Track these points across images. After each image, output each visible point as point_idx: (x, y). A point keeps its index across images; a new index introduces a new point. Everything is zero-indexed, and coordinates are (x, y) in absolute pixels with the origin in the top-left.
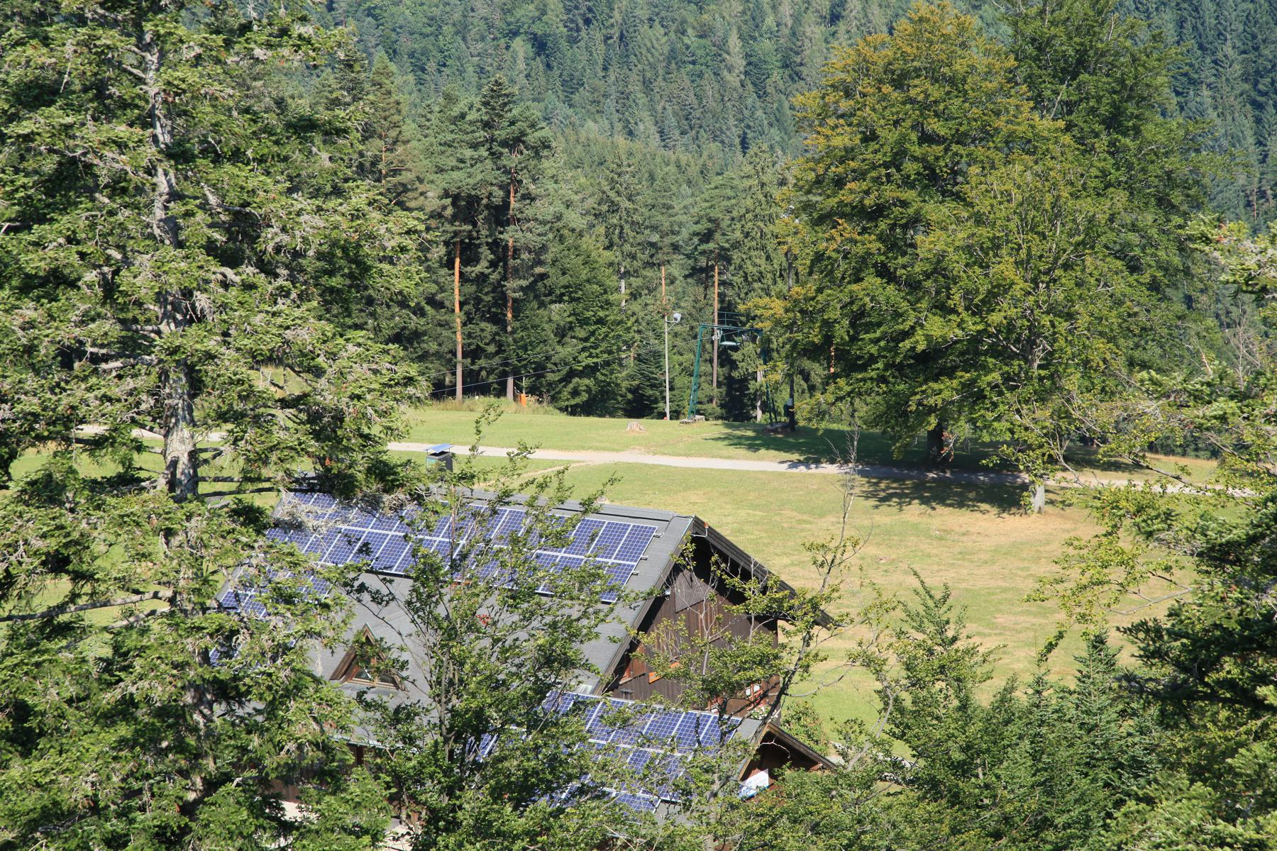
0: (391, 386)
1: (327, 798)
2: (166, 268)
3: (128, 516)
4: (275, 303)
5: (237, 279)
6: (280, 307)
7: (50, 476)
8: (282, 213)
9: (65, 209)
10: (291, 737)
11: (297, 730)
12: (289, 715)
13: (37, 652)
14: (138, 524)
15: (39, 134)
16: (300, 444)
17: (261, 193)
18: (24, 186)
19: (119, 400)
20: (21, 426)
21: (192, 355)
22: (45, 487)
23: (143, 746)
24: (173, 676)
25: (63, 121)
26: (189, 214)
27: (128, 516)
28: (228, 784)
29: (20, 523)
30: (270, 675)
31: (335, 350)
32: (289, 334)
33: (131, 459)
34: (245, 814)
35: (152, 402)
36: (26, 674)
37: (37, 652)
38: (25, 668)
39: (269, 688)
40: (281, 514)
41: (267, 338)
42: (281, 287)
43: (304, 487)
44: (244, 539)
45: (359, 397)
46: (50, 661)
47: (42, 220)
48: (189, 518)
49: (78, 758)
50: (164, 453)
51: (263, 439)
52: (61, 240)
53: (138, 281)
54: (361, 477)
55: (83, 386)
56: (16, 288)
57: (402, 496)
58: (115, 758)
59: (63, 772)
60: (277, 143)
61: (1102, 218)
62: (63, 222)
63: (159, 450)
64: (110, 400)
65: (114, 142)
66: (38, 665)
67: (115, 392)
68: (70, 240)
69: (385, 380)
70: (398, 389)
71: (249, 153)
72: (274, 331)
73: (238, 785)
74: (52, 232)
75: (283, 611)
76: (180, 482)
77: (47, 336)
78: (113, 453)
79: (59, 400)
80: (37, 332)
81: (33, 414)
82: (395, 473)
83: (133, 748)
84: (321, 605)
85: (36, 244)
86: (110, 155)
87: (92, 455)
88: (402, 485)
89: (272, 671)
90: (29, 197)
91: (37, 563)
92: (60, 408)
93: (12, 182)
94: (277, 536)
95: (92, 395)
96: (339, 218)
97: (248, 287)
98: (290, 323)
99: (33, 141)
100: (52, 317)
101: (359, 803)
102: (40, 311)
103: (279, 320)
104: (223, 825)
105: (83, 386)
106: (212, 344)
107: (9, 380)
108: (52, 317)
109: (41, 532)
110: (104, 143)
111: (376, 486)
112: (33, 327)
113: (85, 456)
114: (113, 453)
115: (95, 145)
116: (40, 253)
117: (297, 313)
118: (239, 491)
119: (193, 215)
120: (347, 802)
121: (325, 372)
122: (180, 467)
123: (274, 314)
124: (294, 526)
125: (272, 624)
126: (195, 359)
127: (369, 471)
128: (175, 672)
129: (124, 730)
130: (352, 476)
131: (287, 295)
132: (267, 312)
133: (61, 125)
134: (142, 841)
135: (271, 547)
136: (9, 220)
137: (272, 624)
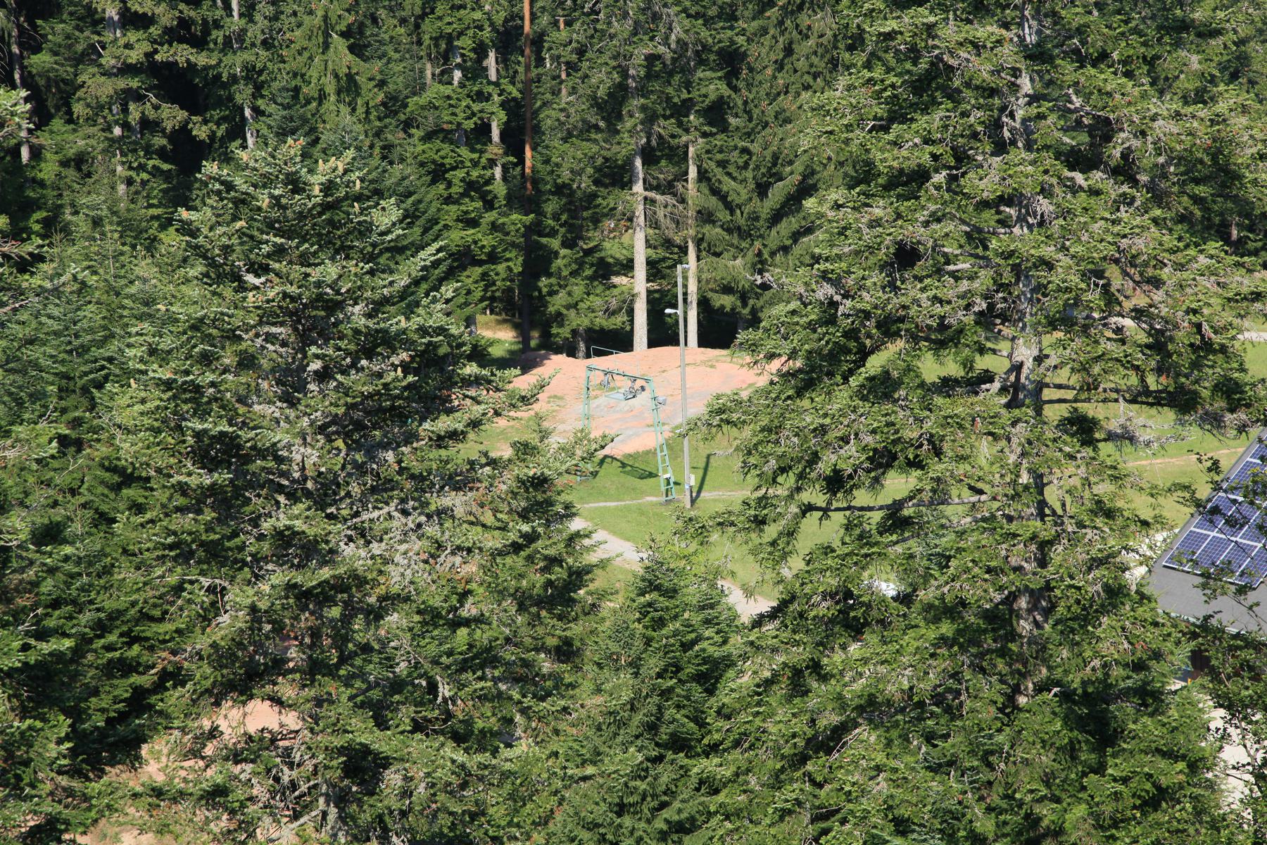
0: (1237, 301)
1: (1145, 719)
2: (1011, 172)
3: (951, 417)
4: (1118, 210)
5: (1084, 184)
6: (1123, 214)
7: (887, 372)
8: (1136, 118)
9: (927, 108)
10: (1097, 654)
11: (1104, 647)
12: (1099, 632)
13: (866, 544)
14: (961, 427)
15: (901, 33)
16: (1126, 356)
17: (1118, 96)
18: (893, 86)
19: (949, 302)
20: (853, 322)
21: (1028, 260)
22: (882, 383)
23: (961, 646)
24: (986, 580)
25: (925, 20)
26: (1041, 117)
27: (951, 417)
28: (1045, 693)
29: (853, 417)
30: (1079, 589)
31: (1183, 261)
32: (1124, 243)
33: (972, 361)
34: (1058, 725)
35: (984, 306)
36: (856, 564)
37: (866, 544)
38: (855, 558)
39: (1078, 602)
40: (1114, 426)
41: (1100, 246)
42: (1124, 194)
43: (1140, 397)
44: (1067, 449)
45: (1195, 312)
46: (879, 554)
47: (904, 120)
48: (1014, 424)
49: (898, 651)
50: (1010, 356)
51: (1089, 348)
52: (917, 140)
53: (982, 185)
54: (1205, 393)
55: (919, 286)
56: (881, 186)
57: (1243, 417)
58: (933, 655)
59: (882, 663)
60: (1145, 44)
61: (57, 157)
62: (922, 121)
63: (1005, 353)
64: (941, 302)
65: (971, 42)
66: (866, 556)
67: (950, 294)
68: (927, 141)
69: (1230, 295)
70: (1245, 304)
71: (1115, 56)
72: (1110, 239)
73: (1055, 695)
74: (910, 133)
75: (1101, 525)
76: (1024, 386)
77: (890, 234)
78: (956, 354)
79: (888, 299)
80: (881, 230)
81: (863, 311)
82: (1242, 392)
83: (952, 646)
84: (1140, 521)
85: (895, 143)
86: (966, 55)
87: (937, 355)
88: (1248, 406)
89: (1081, 584)
90: (895, 96)
91: (864, 457)
92: (890, 307)
93: (882, 81)
94: (1106, 449)
95: (925, 295)
96: (1195, 124)
97: (1095, 192)
98: (1127, 231)
99: (893, 39)
100: (899, 216)
101: (1176, 728)
102: (889, 210)
103: (1116, 229)
104: (1036, 733)
105: (919, 286)
106: (1048, 251)
107: (853, 276)
108: (899, 216)
109: (871, 428)
110: (961, 44)
111: (1220, 404)
112: (880, 226)
113: (929, 355)
114: (956, 354)
115: (952, 45)
116: (895, 152)
117: (1138, 221)
118: (1076, 400)
119: (1044, 117)
120: (1164, 725)
121: (1164, 283)
122: (1025, 371)
123: (1113, 222)
124: (1126, 437)
125: (1089, 537)
126: (1030, 264)
127: (1216, 388)
128: (987, 576)
129: (947, 628)
130: (1196, 393)
131: (1130, 204)
132: (1106, 220)
133: (923, 24)
134: (960, 739)
135: (1094, 458)
136: (875, 118)
137: (1089, 537)
